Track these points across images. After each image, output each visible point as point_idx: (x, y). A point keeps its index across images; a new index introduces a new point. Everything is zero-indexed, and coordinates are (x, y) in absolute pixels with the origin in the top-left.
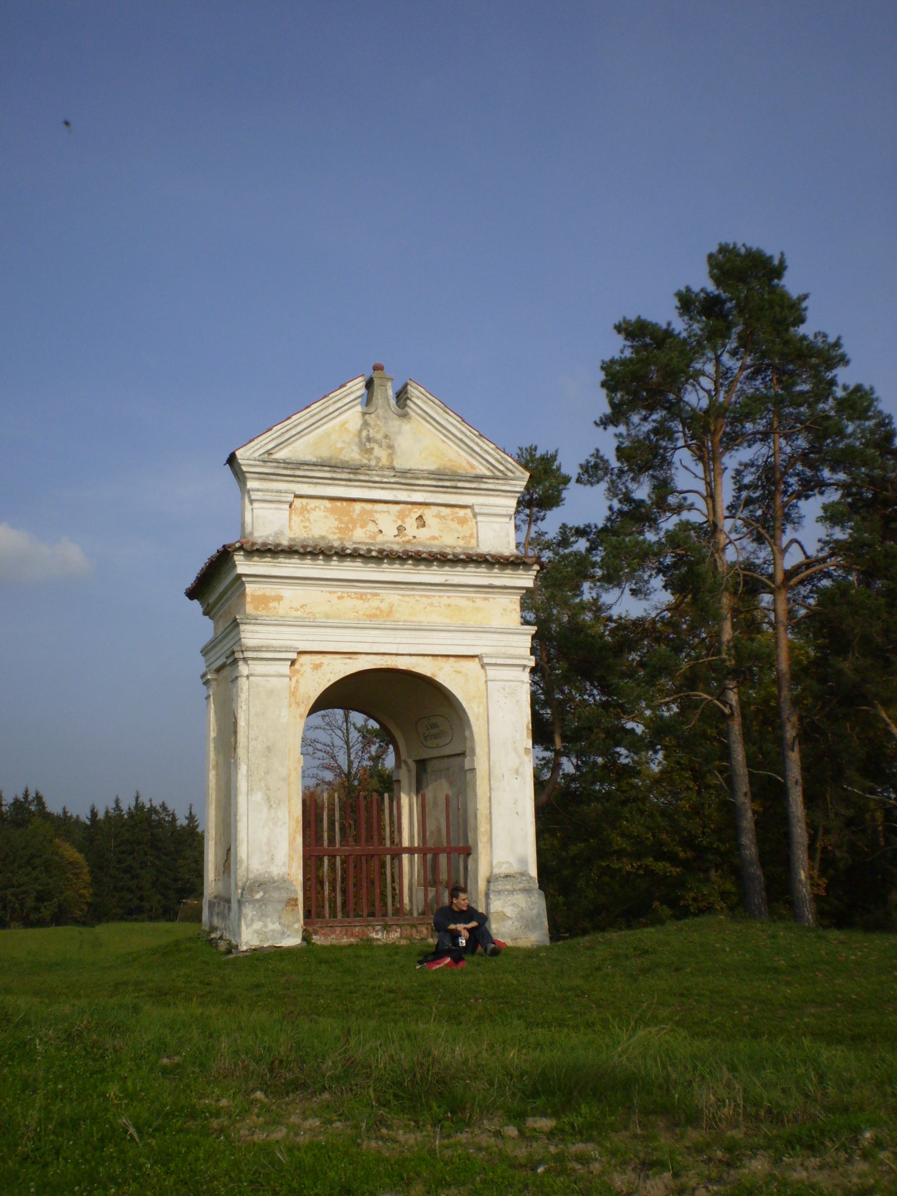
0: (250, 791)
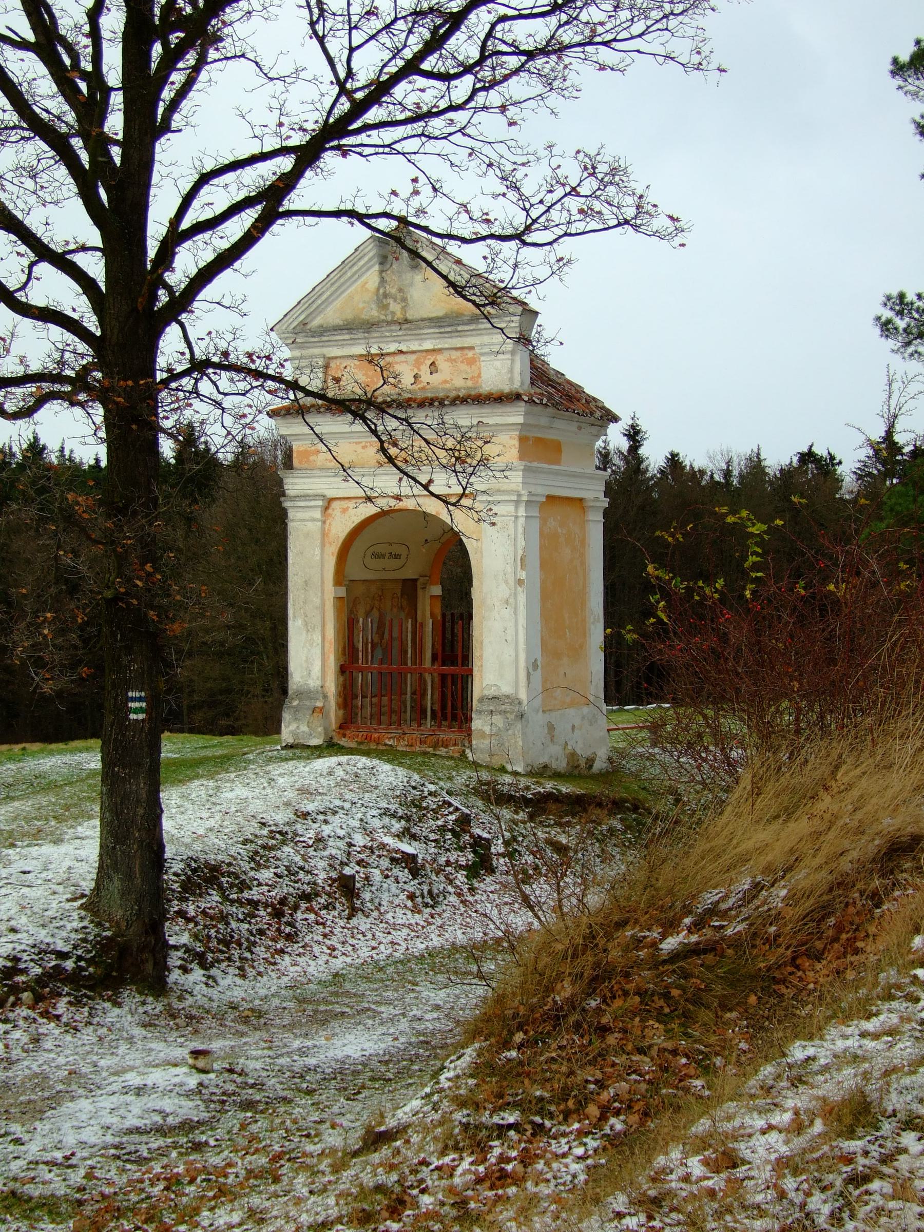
0: (295, 617)
